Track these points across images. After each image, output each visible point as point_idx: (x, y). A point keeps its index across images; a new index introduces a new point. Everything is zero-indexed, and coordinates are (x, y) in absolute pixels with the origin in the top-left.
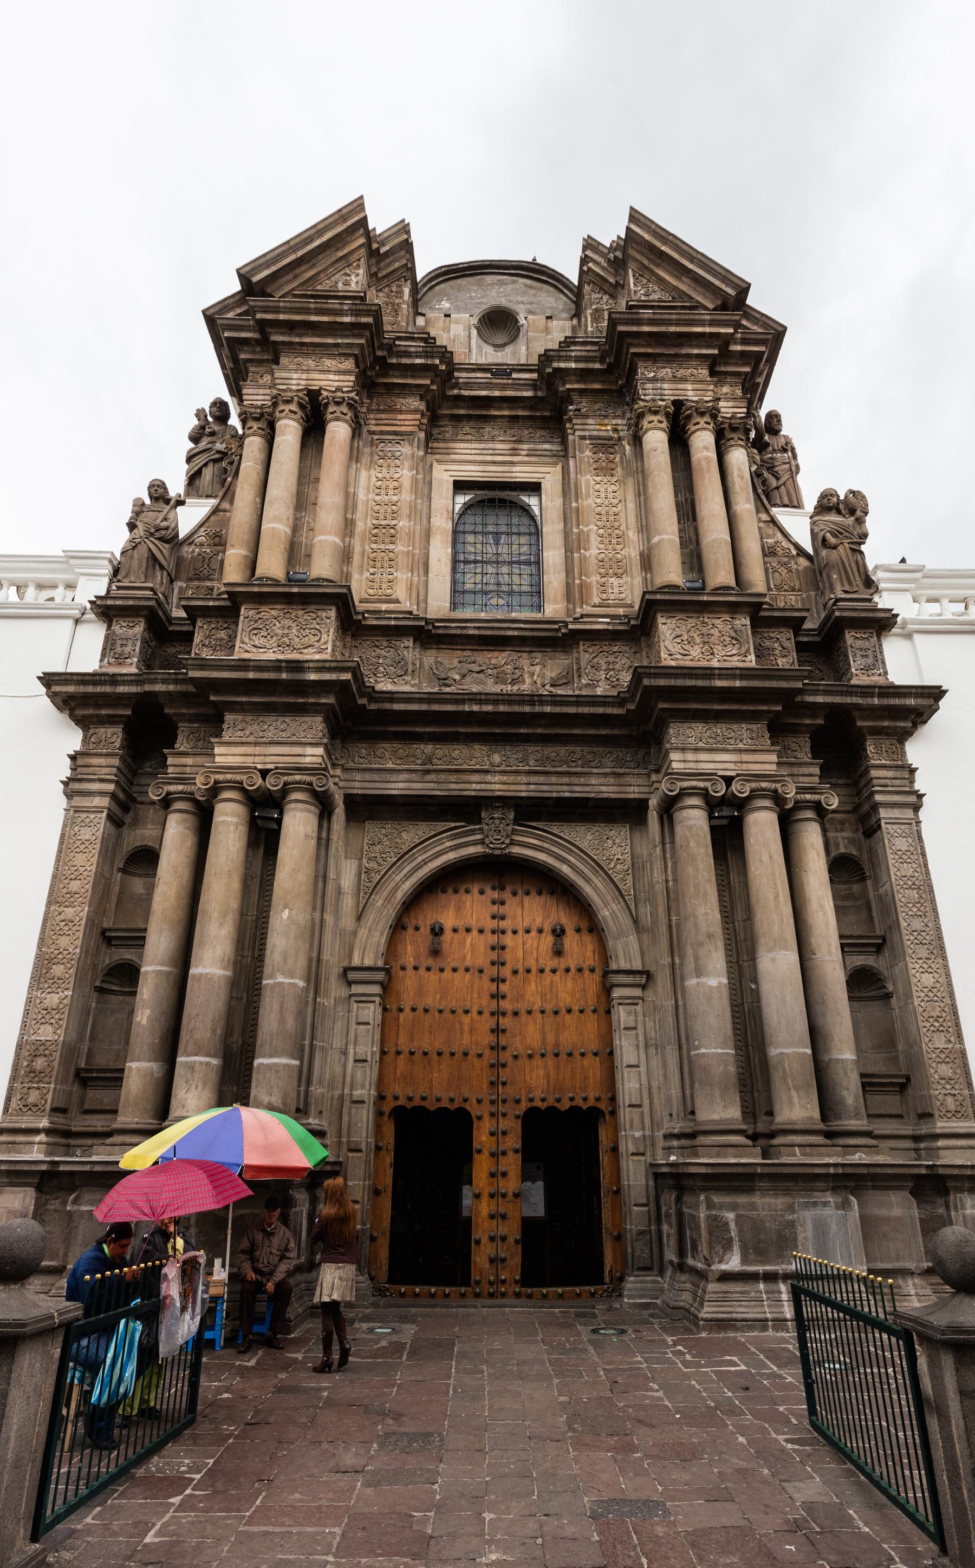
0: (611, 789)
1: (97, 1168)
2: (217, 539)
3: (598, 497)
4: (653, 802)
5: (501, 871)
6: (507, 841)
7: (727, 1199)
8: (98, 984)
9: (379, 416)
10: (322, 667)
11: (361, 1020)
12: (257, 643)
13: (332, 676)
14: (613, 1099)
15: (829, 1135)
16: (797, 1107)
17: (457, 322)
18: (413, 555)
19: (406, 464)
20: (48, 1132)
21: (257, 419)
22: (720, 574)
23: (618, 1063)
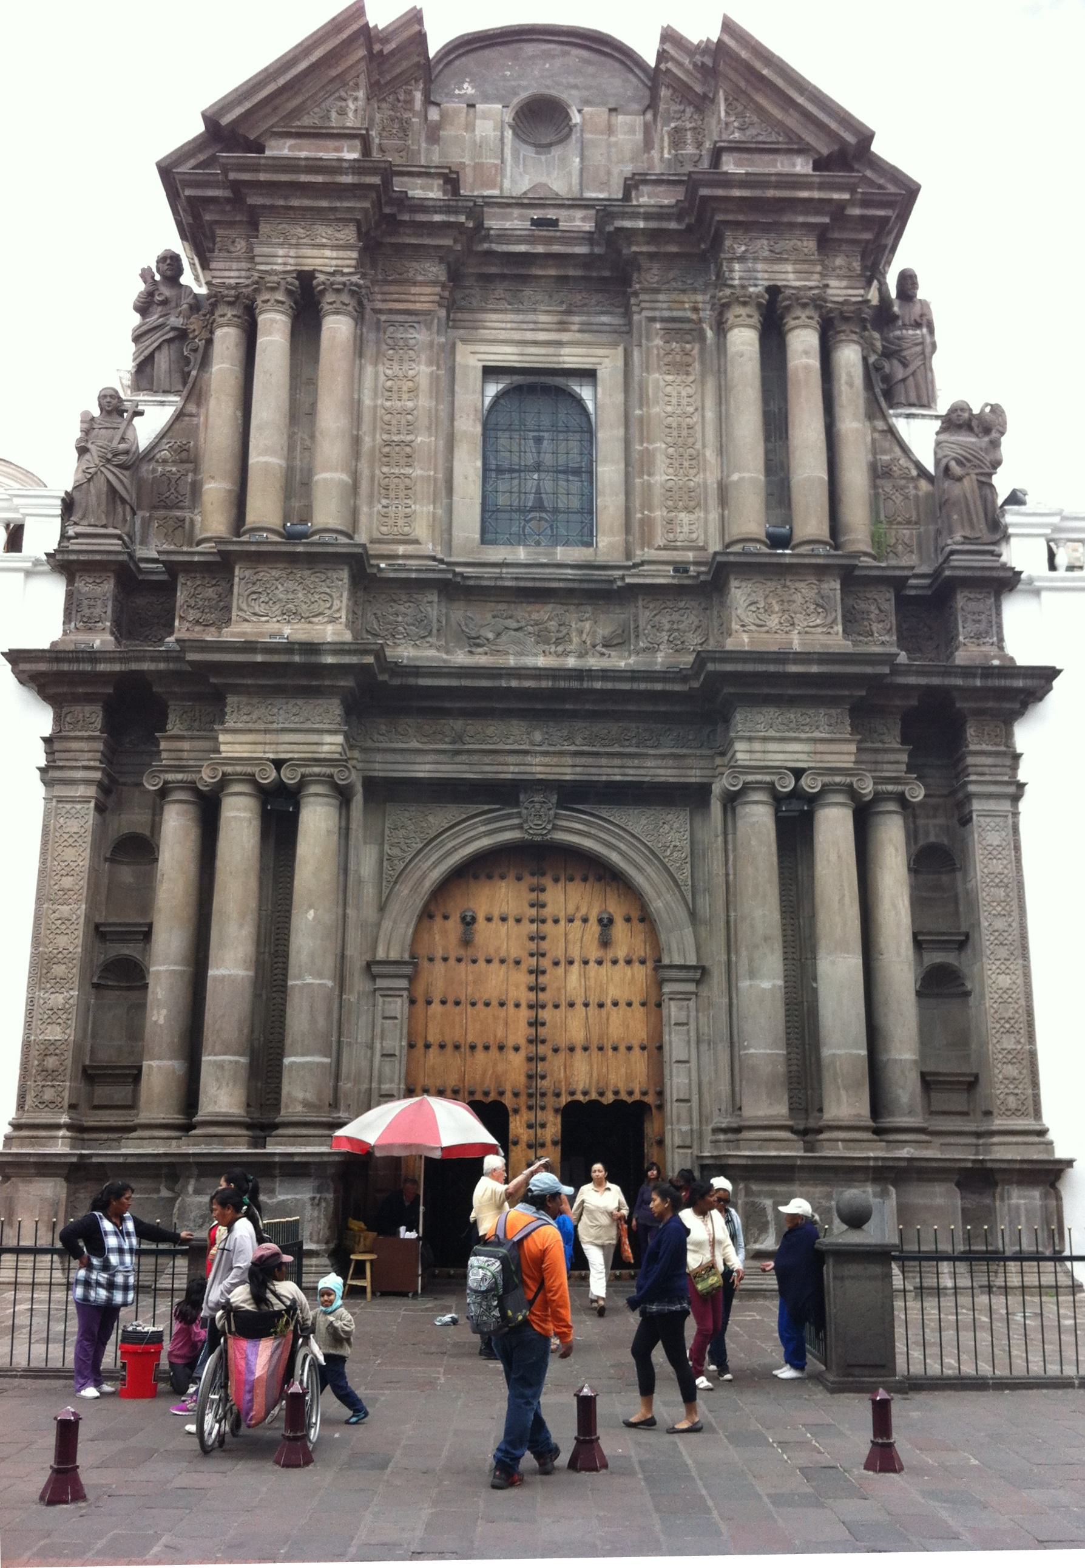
0: (669, 772)
1: (130, 1160)
2: (184, 455)
3: (669, 403)
4: (716, 789)
5: (539, 859)
6: (549, 827)
7: (766, 1188)
8: (95, 980)
9: (386, 289)
10: (339, 648)
11: (387, 1014)
12: (257, 610)
13: (354, 660)
14: (660, 1094)
15: (877, 1131)
16: (845, 1104)
17: (485, 116)
18: (435, 480)
19: (423, 357)
20: (68, 1127)
21: (231, 304)
22: (811, 523)
23: (666, 1058)
